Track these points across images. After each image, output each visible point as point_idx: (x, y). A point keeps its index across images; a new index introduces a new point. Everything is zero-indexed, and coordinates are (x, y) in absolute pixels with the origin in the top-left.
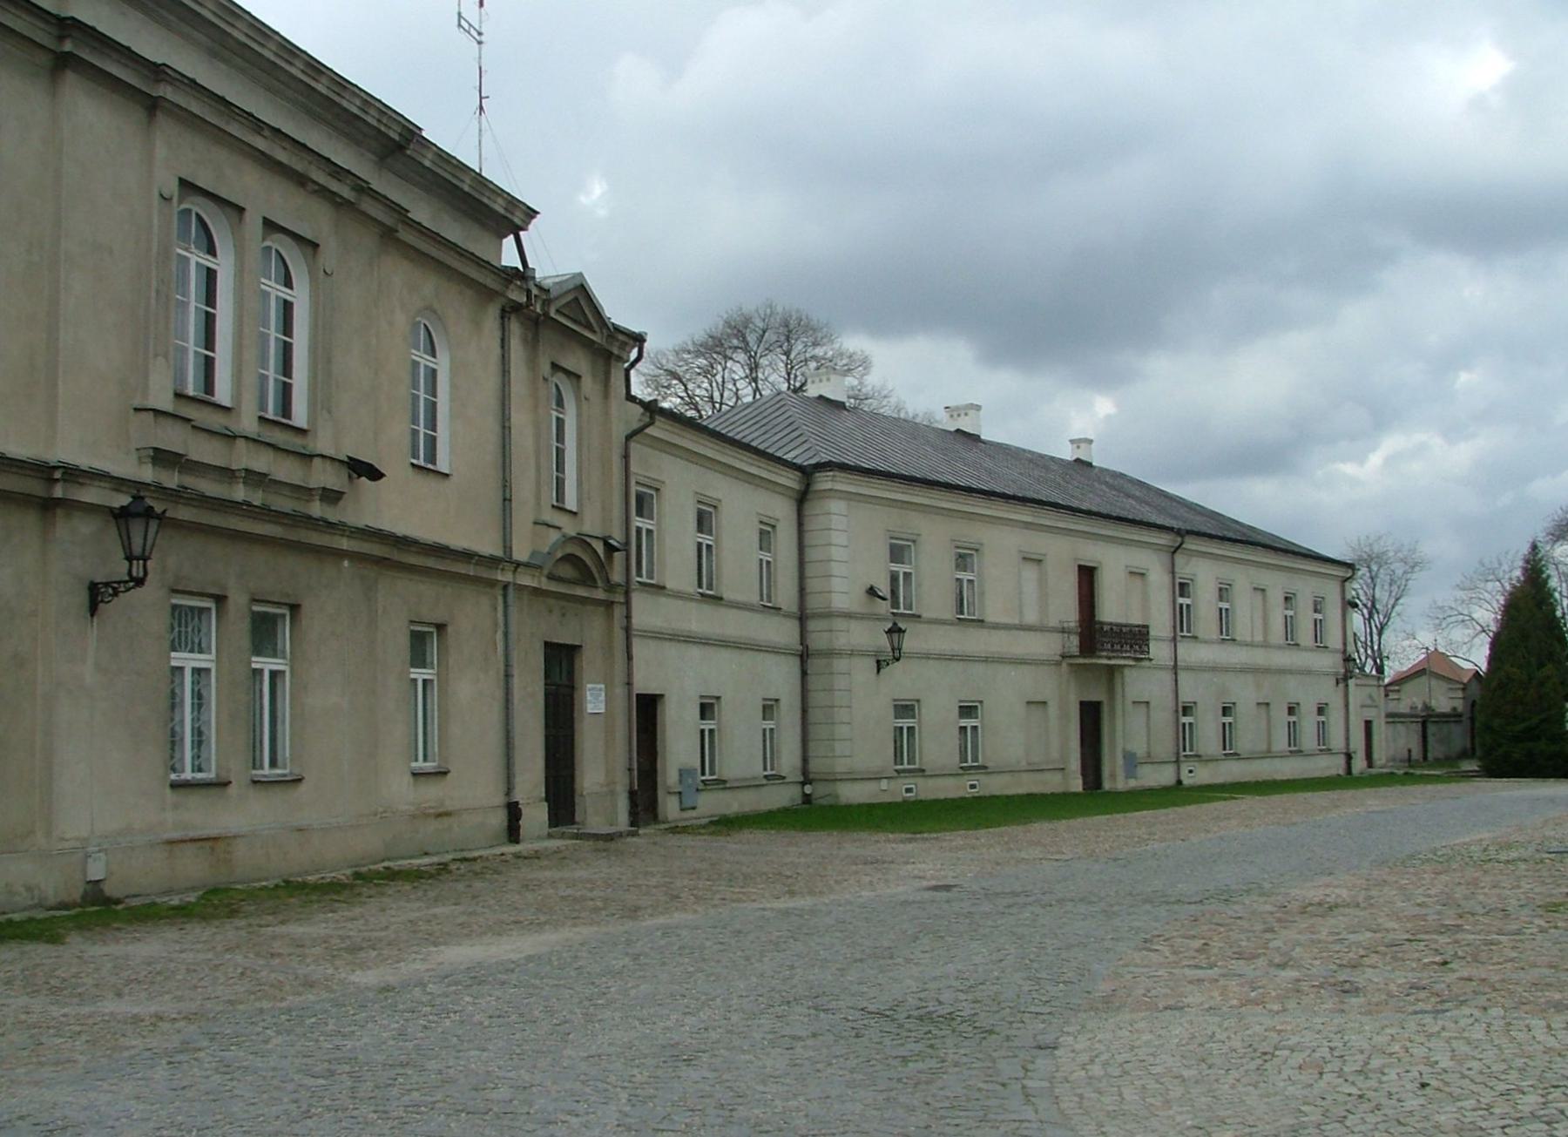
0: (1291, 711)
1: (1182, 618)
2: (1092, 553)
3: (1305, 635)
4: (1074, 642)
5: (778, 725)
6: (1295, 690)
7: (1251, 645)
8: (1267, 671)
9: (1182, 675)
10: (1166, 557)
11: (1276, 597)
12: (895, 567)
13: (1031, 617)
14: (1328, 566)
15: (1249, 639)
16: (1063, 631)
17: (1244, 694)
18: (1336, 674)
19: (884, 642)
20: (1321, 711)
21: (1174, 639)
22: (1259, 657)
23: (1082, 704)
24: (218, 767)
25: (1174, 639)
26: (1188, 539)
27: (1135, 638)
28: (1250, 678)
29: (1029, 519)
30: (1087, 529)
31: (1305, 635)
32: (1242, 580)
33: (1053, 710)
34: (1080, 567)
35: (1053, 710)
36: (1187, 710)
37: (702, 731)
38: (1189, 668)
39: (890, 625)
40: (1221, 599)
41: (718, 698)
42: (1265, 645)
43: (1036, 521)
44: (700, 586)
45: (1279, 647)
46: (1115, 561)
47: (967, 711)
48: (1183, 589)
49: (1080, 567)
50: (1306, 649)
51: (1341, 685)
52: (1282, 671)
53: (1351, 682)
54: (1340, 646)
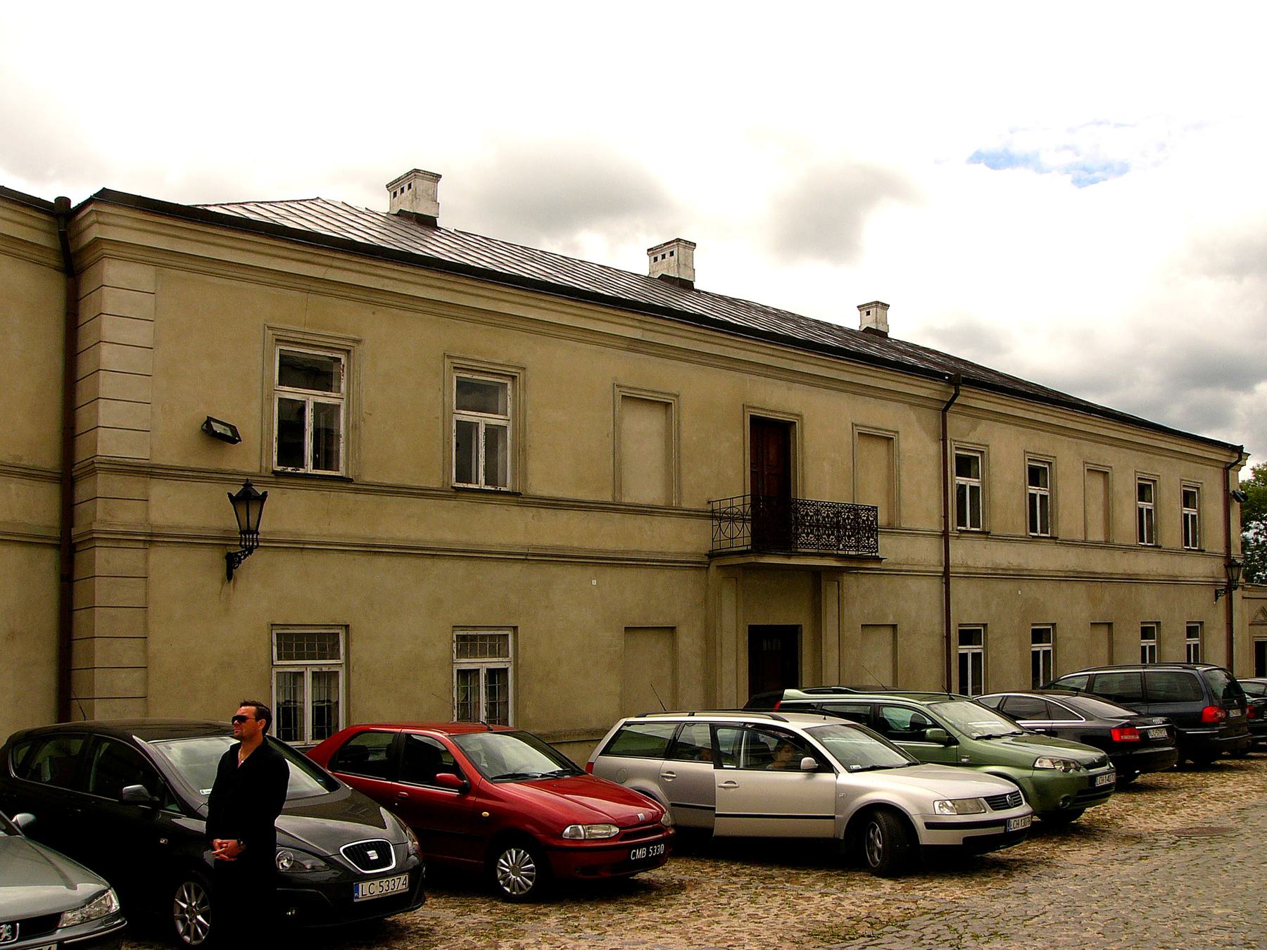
0: (1146, 633)
1: (965, 511)
2: (778, 398)
3: (1171, 533)
4: (740, 535)
5: (1202, 643)
6: (1151, 604)
7: (1086, 544)
8: (1108, 579)
9: (957, 587)
10: (933, 419)
11: (1125, 487)
12: (1032, 490)
13: (1097, 535)
14: (326, 257)
15: (1080, 537)
16: (714, 515)
17: (1070, 611)
18: (1215, 583)
19: (226, 519)
20: (1191, 632)
21: (945, 535)
22: (1099, 562)
23: (750, 627)
24: (516, 722)
25: (945, 535)
26: (964, 391)
27: (856, 526)
28: (1080, 589)
29: (637, 334)
30: (716, 350)
31: (1171, 533)
32: (1069, 460)
33: (689, 641)
34: (755, 421)
35: (689, 641)
36: (968, 636)
37: (1189, 646)
38: (969, 575)
39: (236, 490)
40: (1142, 498)
41: (1201, 623)
42: (1107, 545)
43: (649, 337)
44: (1033, 529)
45: (1178, 553)
46: (1069, 460)
47: (1038, 636)
48: (966, 465)
49: (755, 421)
50: (1171, 552)
51: (1222, 599)
52: (1132, 579)
53: (1237, 595)
54: (1221, 549)
